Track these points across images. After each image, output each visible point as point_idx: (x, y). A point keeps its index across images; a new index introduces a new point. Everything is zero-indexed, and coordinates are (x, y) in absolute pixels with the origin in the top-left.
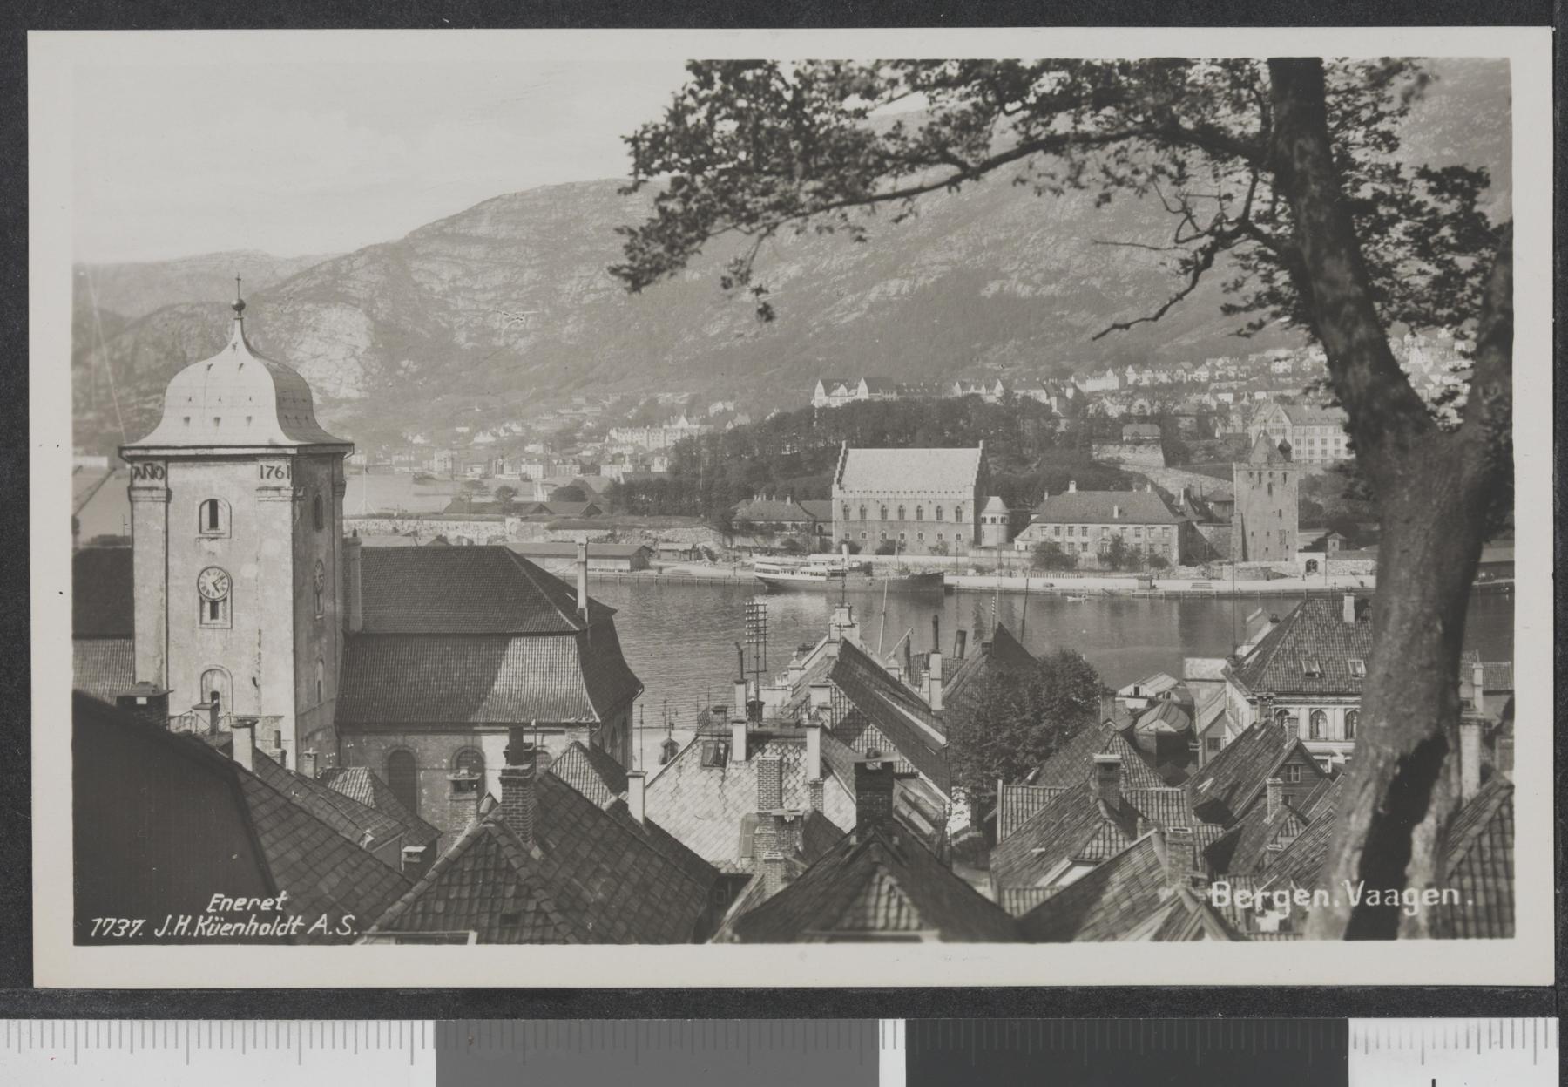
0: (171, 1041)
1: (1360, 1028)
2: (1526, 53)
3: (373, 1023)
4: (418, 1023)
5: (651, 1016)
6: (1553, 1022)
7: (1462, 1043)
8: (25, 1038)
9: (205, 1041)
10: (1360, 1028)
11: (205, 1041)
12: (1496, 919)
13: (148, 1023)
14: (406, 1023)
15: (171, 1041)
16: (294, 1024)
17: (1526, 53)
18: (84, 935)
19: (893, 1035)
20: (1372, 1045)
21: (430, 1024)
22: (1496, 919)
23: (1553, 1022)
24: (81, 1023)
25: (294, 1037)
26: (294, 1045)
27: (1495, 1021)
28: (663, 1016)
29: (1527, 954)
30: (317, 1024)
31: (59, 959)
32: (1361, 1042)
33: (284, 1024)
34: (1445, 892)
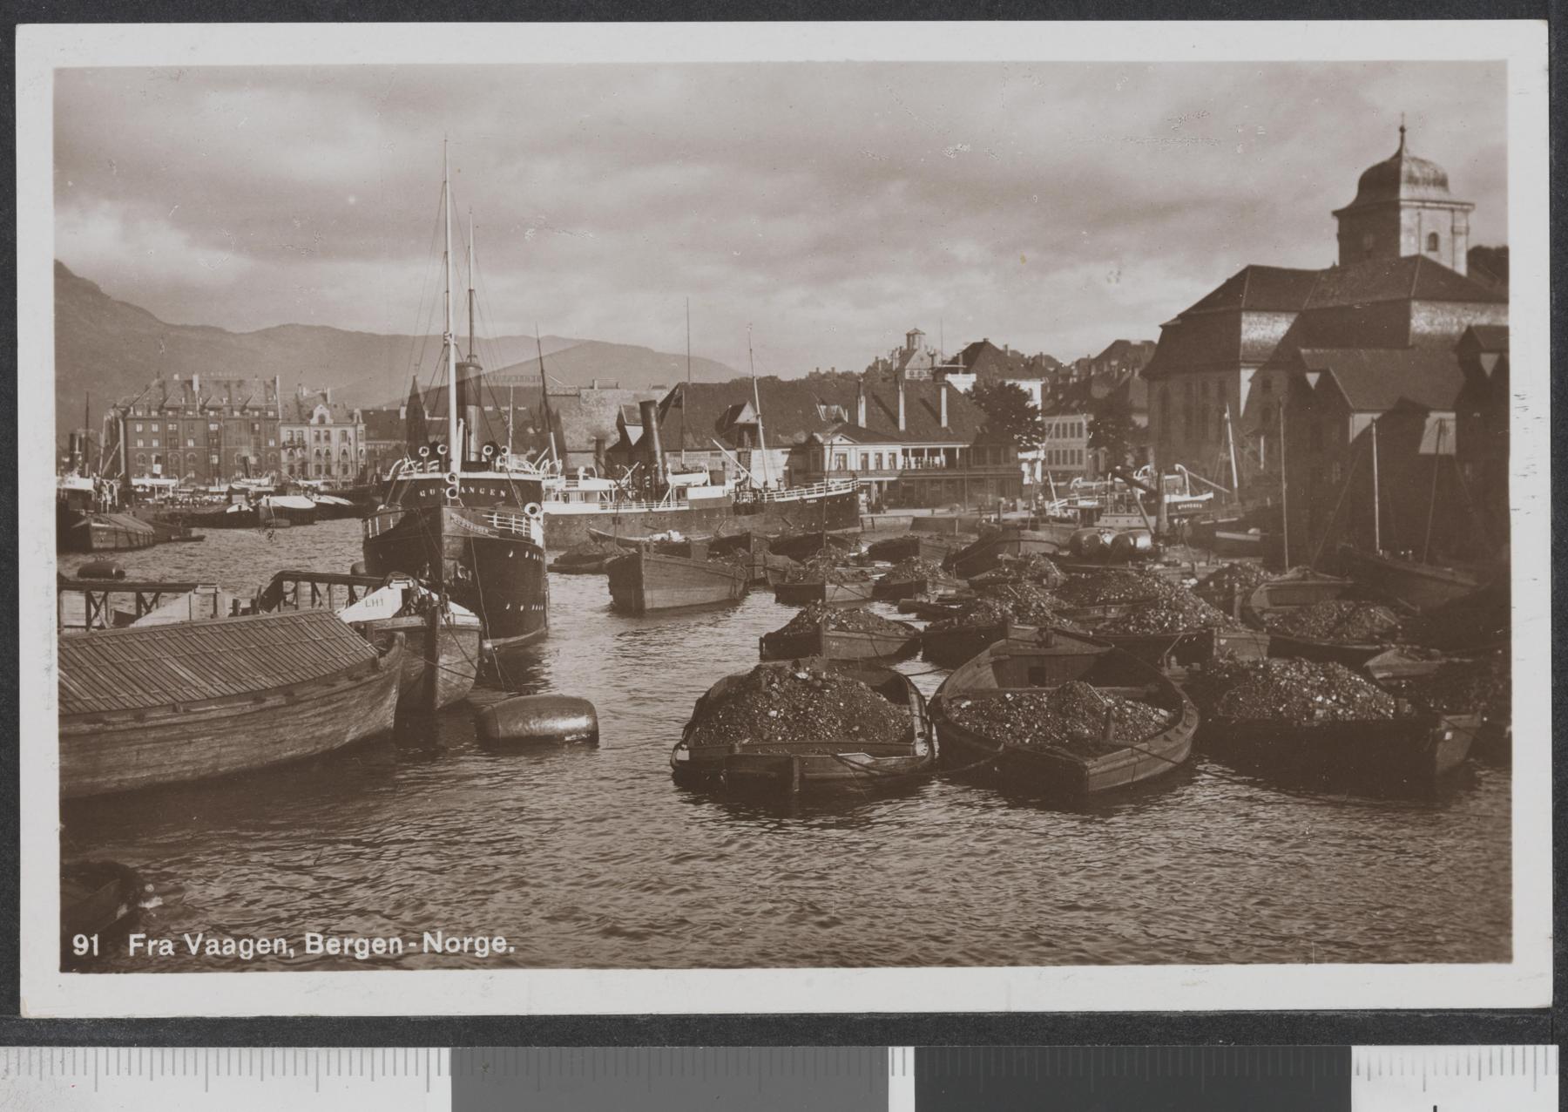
0: (190, 1068)
1: (1363, 1056)
2: (1523, 45)
3: (389, 1051)
4: (433, 1051)
5: (659, 1043)
6: (1553, 1050)
7: (1463, 1070)
8: (213, 1066)
9: (224, 1068)
10: (1363, 1056)
11: (224, 1068)
12: (1490, 941)
13: (168, 1051)
14: (422, 1051)
15: (190, 1068)
16: (312, 1051)
17: (1523, 45)
18: (70, 962)
19: (902, 1062)
20: (1375, 1072)
21: (446, 1052)
22: (1490, 941)
23: (1553, 1050)
24: (102, 1050)
25: (312, 1064)
26: (312, 1074)
27: (1496, 1048)
28: (672, 1043)
29: (1525, 977)
30: (301, 1051)
31: (45, 988)
32: (1364, 1069)
33: (301, 1051)
34: (276, 942)
